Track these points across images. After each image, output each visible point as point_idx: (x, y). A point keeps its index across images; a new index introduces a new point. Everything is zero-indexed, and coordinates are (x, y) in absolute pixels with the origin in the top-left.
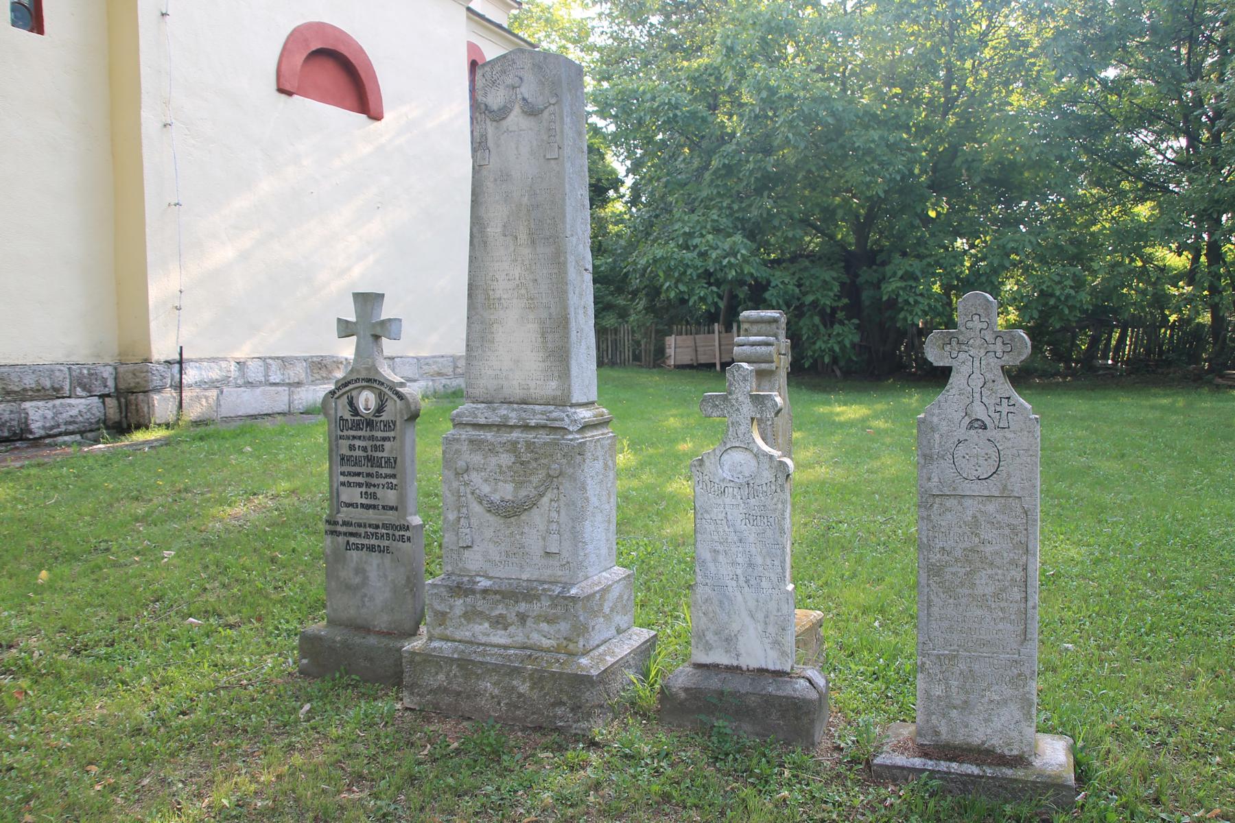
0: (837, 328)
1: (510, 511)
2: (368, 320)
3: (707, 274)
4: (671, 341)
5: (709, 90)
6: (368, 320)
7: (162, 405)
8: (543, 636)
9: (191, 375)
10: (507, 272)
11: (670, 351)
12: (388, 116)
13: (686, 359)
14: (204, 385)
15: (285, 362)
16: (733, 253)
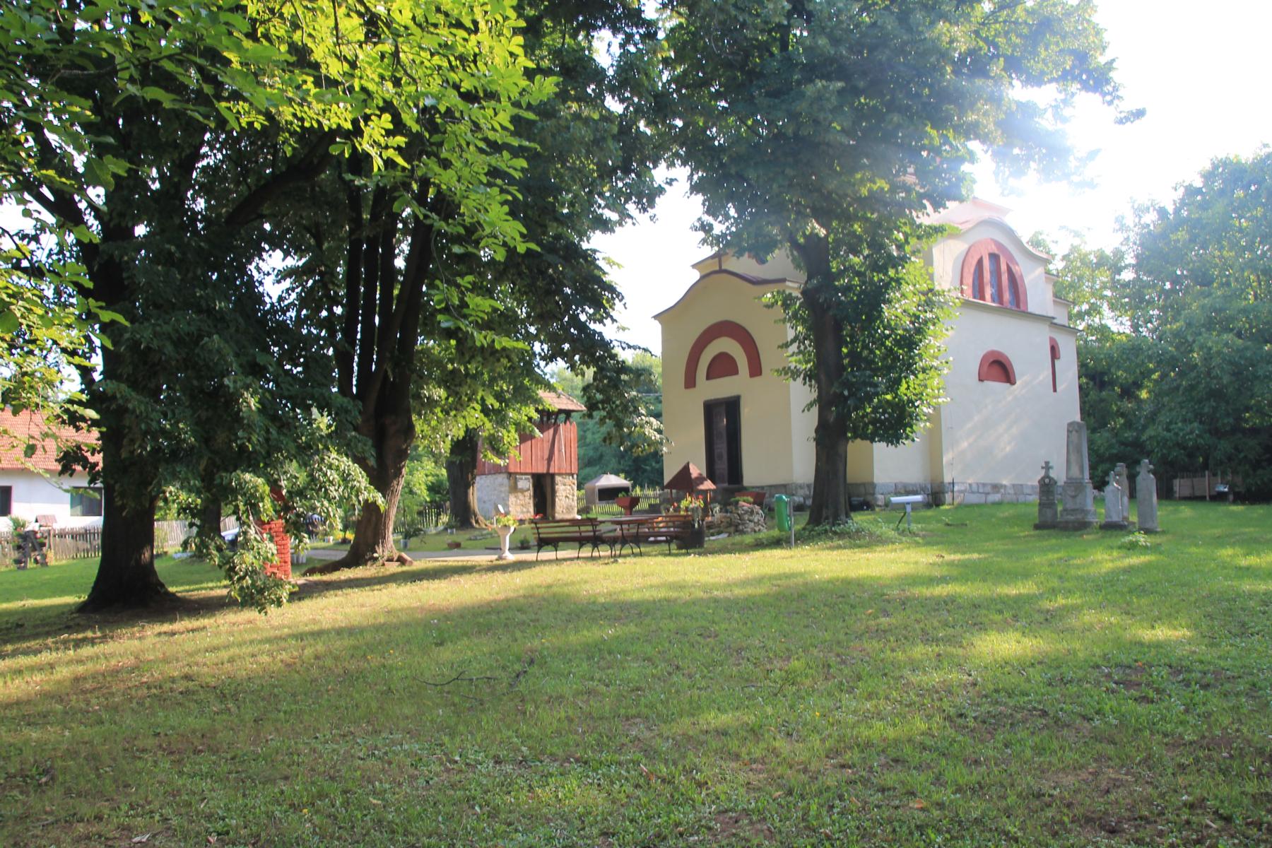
0: (1260, 472)
1: (1074, 497)
2: (1047, 467)
3: (1178, 444)
4: (1177, 482)
5: (1185, 345)
6: (1047, 467)
7: (948, 497)
8: (1079, 516)
9: (956, 488)
10: (1073, 458)
11: (1176, 488)
12: (1018, 383)
13: (1187, 493)
14: (960, 492)
15: (984, 485)
16: (1192, 432)
